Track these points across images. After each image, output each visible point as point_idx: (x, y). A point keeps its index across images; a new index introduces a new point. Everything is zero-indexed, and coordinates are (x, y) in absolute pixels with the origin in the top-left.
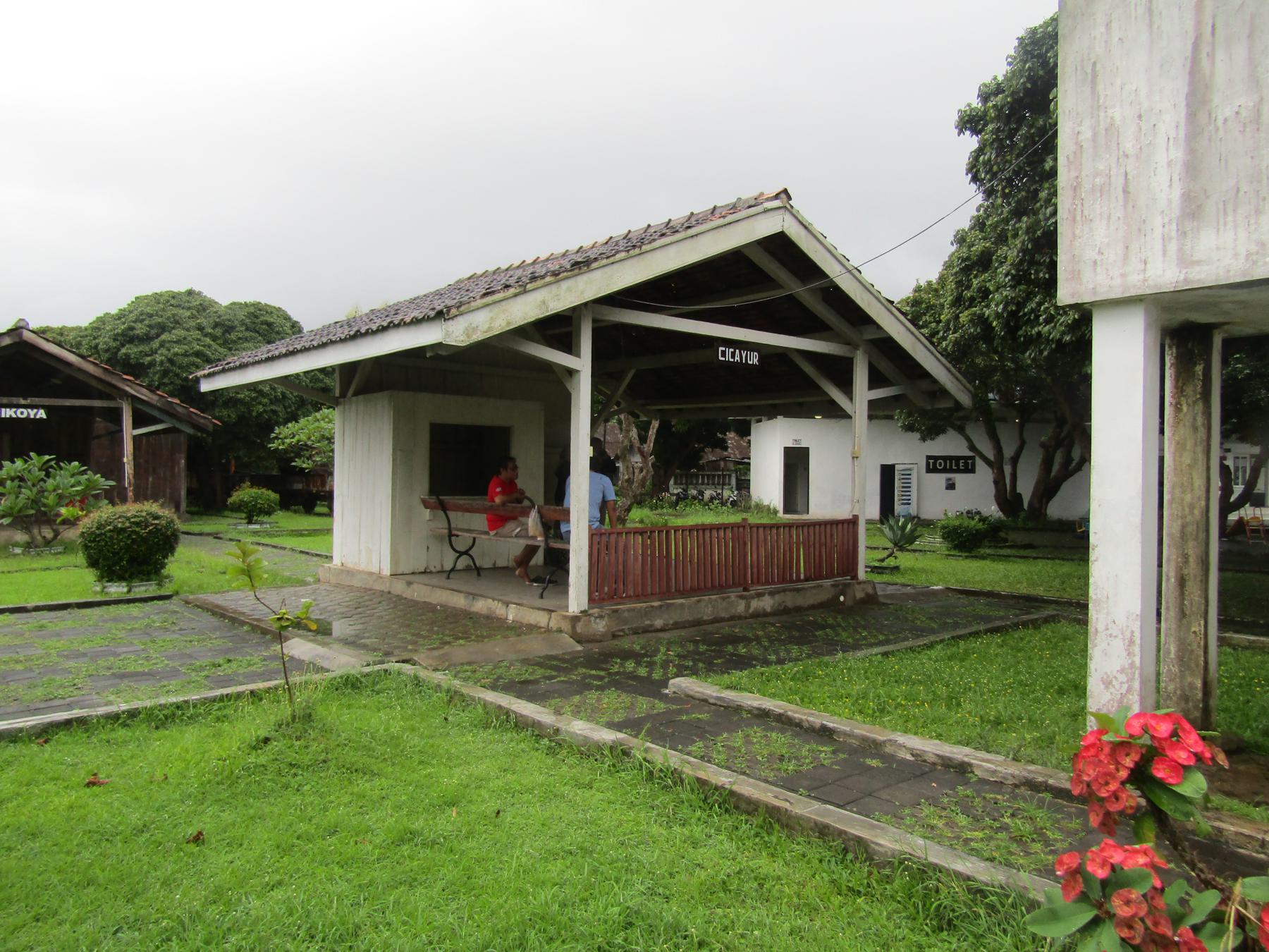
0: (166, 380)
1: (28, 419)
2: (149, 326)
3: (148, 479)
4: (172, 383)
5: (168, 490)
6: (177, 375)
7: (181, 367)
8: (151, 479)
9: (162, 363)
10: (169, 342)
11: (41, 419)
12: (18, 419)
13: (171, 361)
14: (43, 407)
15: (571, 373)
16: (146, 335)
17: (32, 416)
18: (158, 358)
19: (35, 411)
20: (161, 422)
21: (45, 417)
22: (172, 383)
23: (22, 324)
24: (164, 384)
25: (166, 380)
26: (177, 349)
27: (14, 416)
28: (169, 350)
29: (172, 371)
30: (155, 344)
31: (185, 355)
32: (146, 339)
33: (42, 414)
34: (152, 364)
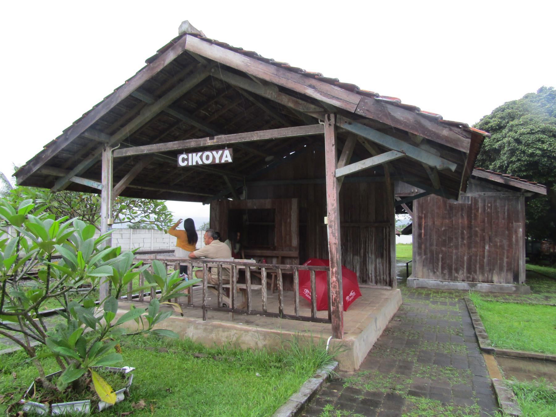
0: (514, 159)
1: (213, 166)
2: (501, 118)
3: (484, 248)
4: (519, 160)
5: (505, 260)
6: (524, 152)
7: (528, 145)
8: (487, 247)
9: (509, 143)
10: (517, 125)
11: (227, 164)
12: (204, 166)
13: (518, 141)
14: (229, 146)
15: (527, 262)
16: (498, 125)
17: (217, 161)
18: (505, 140)
19: (220, 152)
20: (382, 150)
21: (230, 160)
22: (519, 160)
23: (185, 28)
24: (512, 162)
25: (514, 159)
26: (522, 130)
27: (200, 163)
28: (516, 133)
29: (517, 149)
30: (504, 131)
31: (531, 133)
32: (500, 128)
33: (227, 156)
34: (501, 147)
